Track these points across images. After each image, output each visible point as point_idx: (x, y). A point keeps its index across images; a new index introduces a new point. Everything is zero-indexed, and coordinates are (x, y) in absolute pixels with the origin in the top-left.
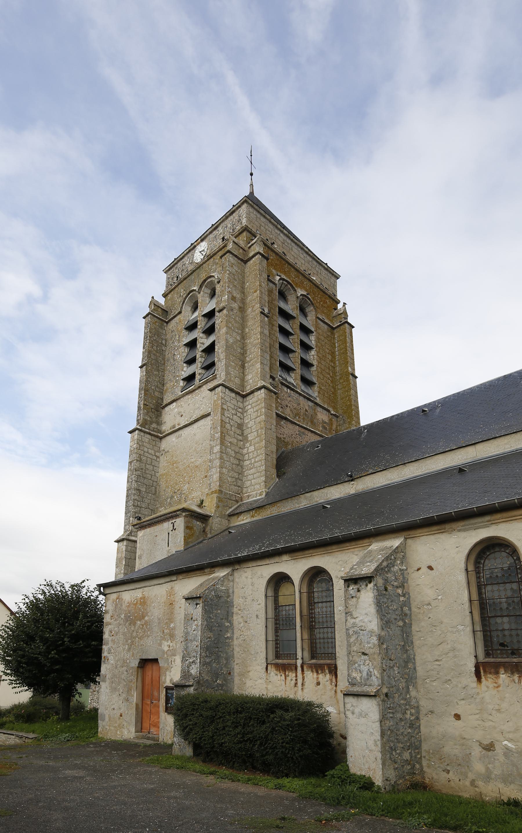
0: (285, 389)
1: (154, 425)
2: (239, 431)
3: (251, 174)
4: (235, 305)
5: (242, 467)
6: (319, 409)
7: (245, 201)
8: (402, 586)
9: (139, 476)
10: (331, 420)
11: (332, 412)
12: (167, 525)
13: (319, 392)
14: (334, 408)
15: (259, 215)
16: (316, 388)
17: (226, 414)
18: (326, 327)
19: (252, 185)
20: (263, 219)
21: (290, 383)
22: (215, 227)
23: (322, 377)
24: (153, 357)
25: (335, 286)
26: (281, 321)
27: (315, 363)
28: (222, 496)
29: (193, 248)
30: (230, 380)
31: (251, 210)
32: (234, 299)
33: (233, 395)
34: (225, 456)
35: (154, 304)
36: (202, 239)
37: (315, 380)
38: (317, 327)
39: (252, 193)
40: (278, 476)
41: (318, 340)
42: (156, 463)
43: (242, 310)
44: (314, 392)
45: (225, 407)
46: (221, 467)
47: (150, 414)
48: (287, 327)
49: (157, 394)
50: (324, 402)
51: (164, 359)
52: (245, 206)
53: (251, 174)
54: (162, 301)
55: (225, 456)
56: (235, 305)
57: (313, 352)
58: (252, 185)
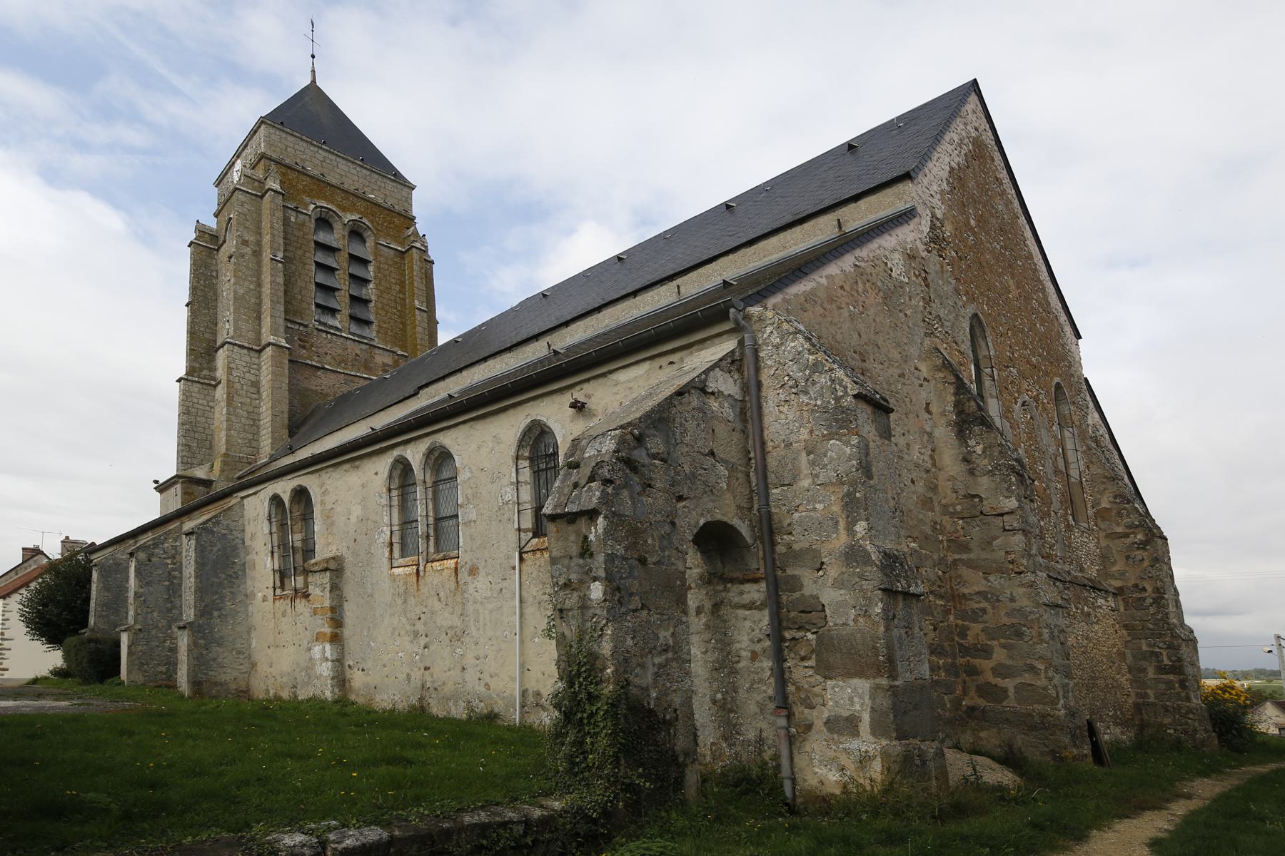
0: (324, 335)
1: (205, 372)
2: (253, 390)
3: (313, 57)
4: (248, 250)
5: (258, 427)
6: (377, 351)
7: (262, 122)
8: (173, 557)
9: (187, 431)
10: (396, 361)
11: (400, 352)
12: (173, 490)
13: (378, 332)
14: (403, 347)
15: (284, 135)
16: (374, 327)
17: (235, 373)
18: (392, 252)
19: (313, 71)
20: (290, 138)
21: (331, 327)
22: (245, 145)
23: (383, 313)
24: (199, 293)
25: (408, 200)
26: (321, 257)
27: (373, 298)
28: (229, 459)
29: (231, 165)
30: (240, 335)
31: (272, 130)
32: (245, 243)
33: (245, 351)
34: (233, 418)
35: (201, 231)
36: (238, 155)
37: (372, 318)
38: (376, 255)
39: (314, 81)
40: (290, 436)
41: (378, 269)
42: (210, 415)
43: (257, 254)
44: (371, 332)
45: (233, 366)
46: (228, 429)
47: (200, 360)
48: (330, 262)
49: (207, 336)
50: (386, 343)
51: (215, 294)
52: (263, 126)
53: (313, 57)
54: (212, 223)
55: (233, 418)
56: (248, 250)
57: (371, 286)
58: (313, 71)
